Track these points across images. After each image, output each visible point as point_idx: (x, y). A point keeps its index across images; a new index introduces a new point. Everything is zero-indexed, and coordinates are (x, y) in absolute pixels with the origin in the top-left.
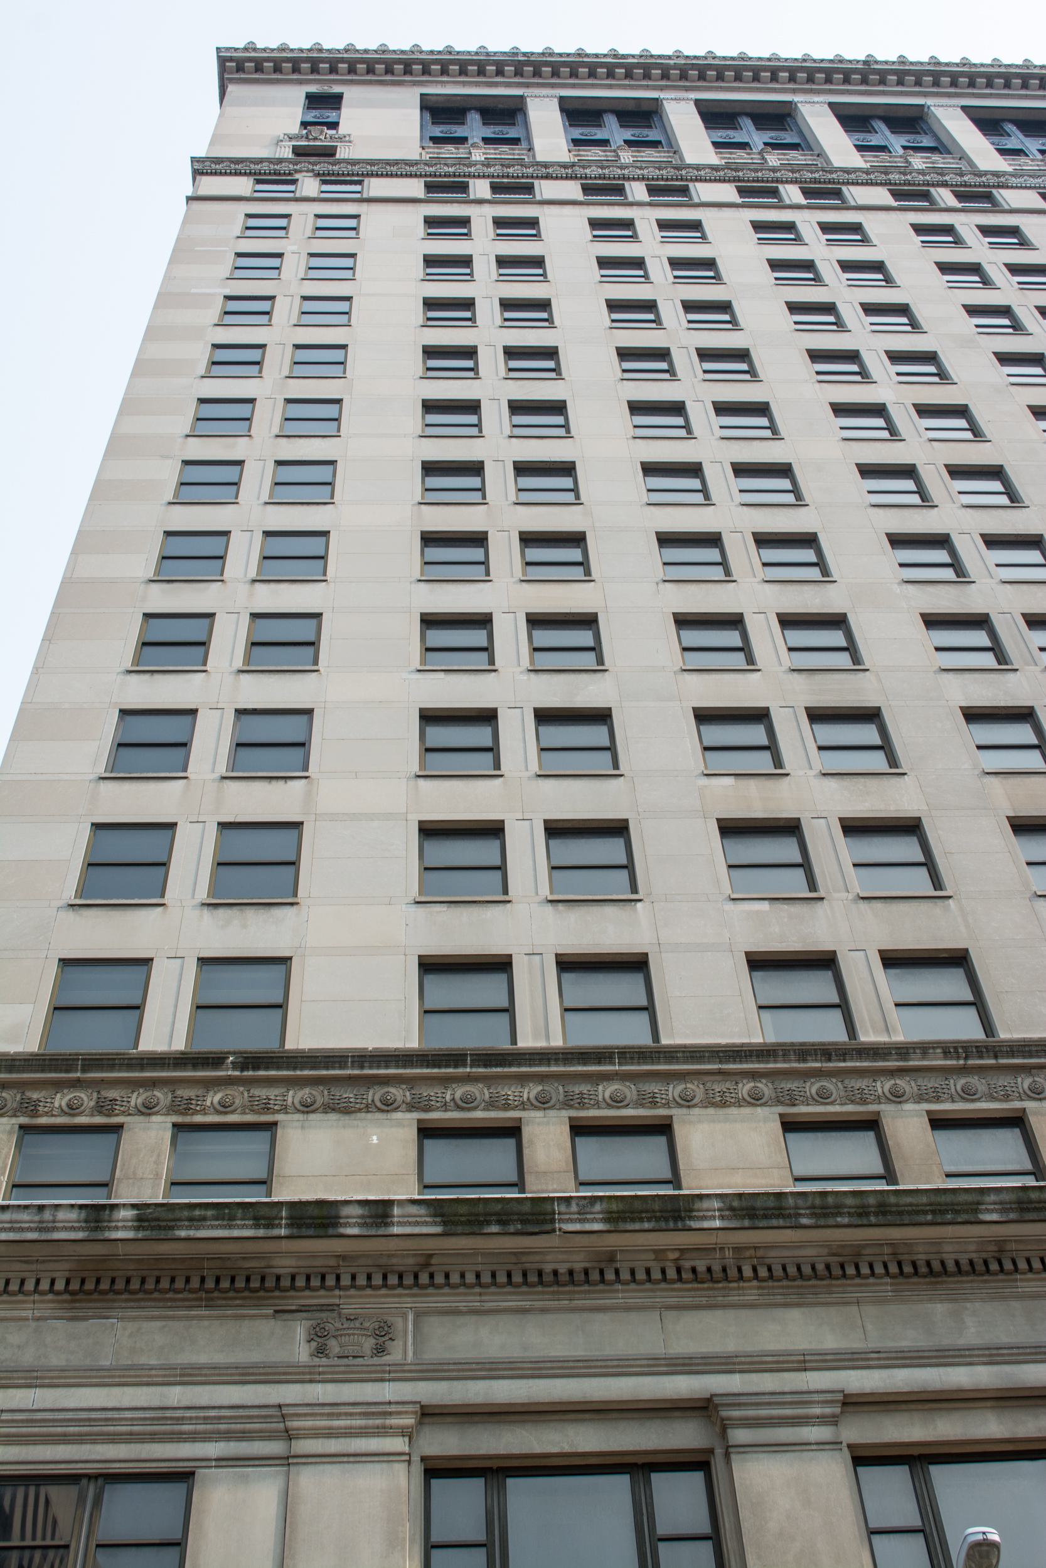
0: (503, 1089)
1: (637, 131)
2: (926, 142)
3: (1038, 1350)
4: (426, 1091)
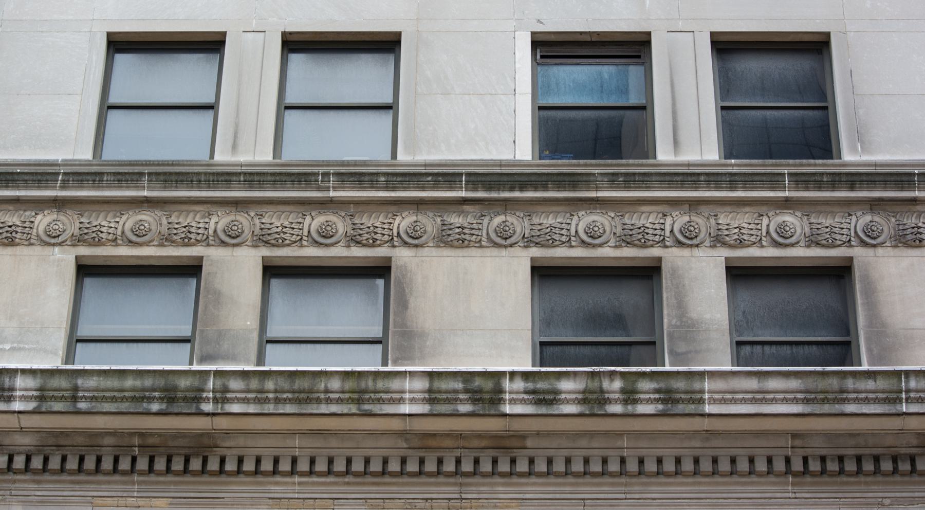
4: (368, 220)
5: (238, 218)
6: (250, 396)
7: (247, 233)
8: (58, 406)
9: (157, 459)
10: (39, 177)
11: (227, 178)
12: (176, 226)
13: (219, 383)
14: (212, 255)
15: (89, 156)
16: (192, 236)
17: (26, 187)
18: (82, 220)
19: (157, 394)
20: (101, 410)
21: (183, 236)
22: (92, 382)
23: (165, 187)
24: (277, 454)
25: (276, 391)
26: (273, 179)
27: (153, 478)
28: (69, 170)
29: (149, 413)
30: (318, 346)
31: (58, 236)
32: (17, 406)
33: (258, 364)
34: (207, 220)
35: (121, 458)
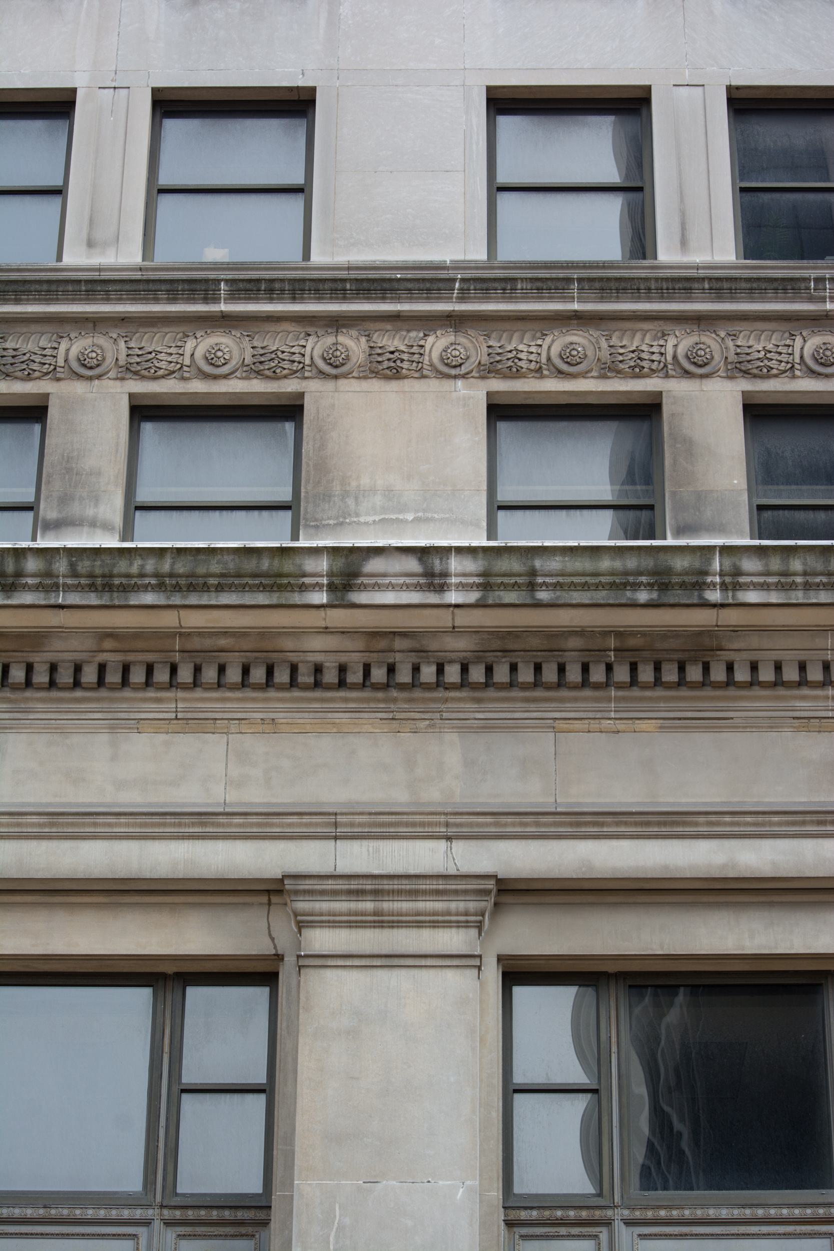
0: (621, 339)
3: (822, 817)
5: (704, 339)
6: (772, 580)
7: (109, 361)
8: (510, 597)
9: (640, 668)
10: (428, 285)
11: (687, 285)
12: (622, 351)
13: (728, 563)
14: (674, 389)
15: (484, 257)
16: (644, 364)
17: (411, 298)
18: (491, 343)
19: (644, 579)
20: (569, 602)
21: (633, 364)
22: (555, 564)
23: (602, 297)
24: (802, 658)
25: (805, 574)
26: (748, 286)
27: (636, 692)
28: (469, 274)
29: (634, 605)
30: (519, 514)
31: (460, 365)
32: (453, 597)
33: (123, 539)
34: (662, 342)
35: (591, 667)
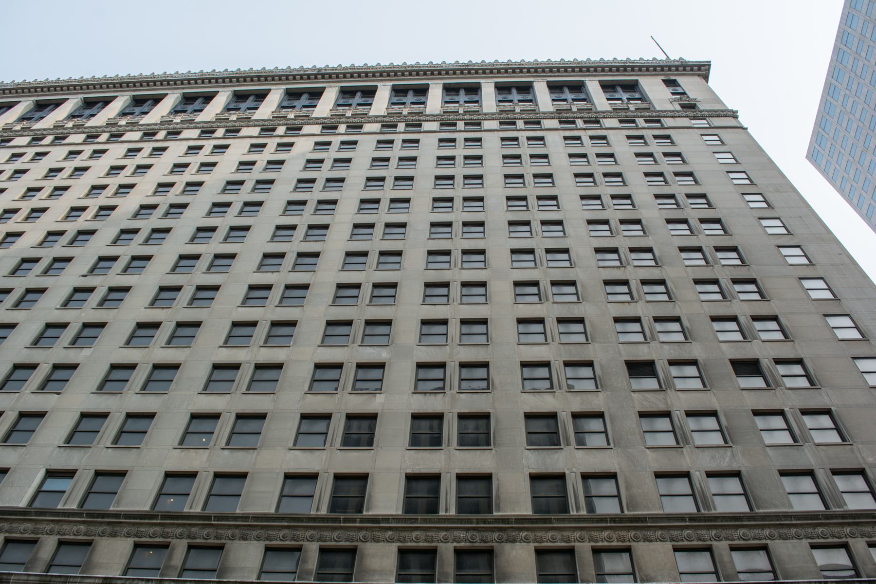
1: (557, 95)
2: (637, 96)
